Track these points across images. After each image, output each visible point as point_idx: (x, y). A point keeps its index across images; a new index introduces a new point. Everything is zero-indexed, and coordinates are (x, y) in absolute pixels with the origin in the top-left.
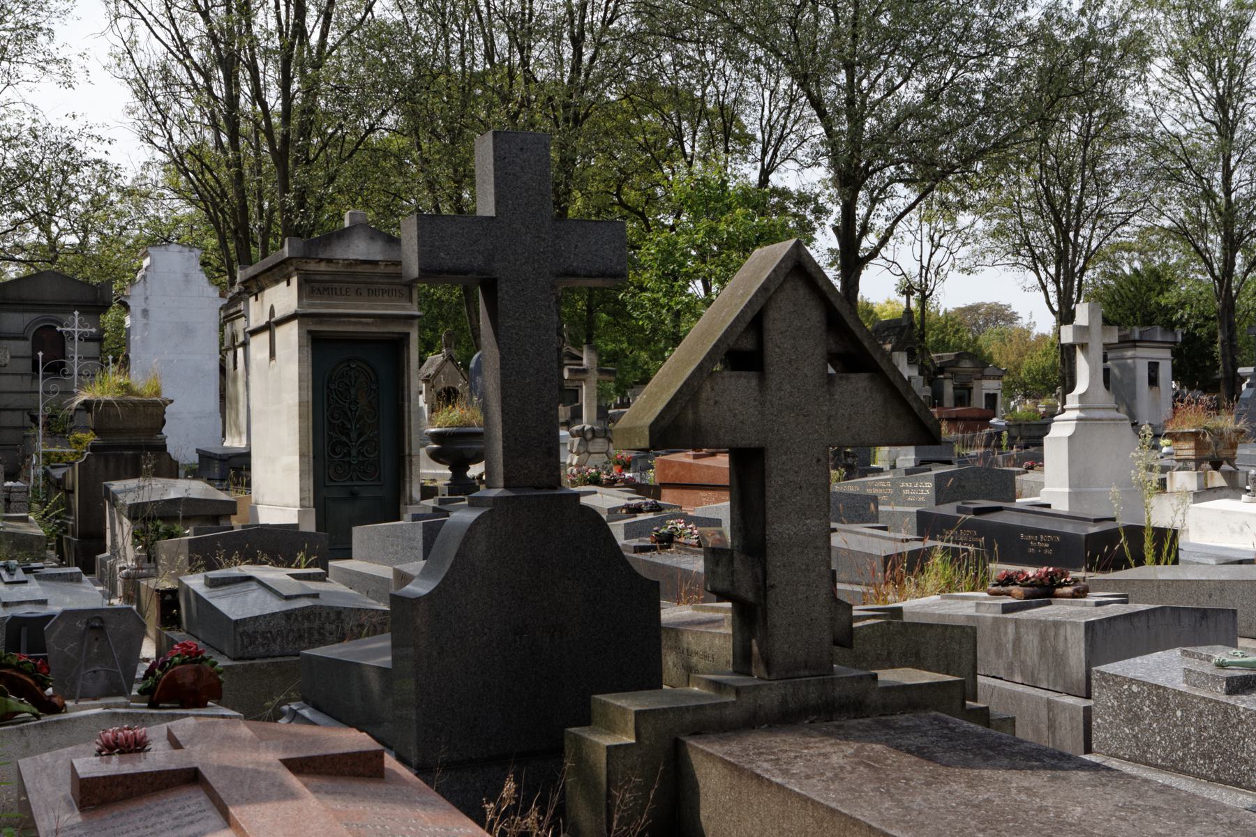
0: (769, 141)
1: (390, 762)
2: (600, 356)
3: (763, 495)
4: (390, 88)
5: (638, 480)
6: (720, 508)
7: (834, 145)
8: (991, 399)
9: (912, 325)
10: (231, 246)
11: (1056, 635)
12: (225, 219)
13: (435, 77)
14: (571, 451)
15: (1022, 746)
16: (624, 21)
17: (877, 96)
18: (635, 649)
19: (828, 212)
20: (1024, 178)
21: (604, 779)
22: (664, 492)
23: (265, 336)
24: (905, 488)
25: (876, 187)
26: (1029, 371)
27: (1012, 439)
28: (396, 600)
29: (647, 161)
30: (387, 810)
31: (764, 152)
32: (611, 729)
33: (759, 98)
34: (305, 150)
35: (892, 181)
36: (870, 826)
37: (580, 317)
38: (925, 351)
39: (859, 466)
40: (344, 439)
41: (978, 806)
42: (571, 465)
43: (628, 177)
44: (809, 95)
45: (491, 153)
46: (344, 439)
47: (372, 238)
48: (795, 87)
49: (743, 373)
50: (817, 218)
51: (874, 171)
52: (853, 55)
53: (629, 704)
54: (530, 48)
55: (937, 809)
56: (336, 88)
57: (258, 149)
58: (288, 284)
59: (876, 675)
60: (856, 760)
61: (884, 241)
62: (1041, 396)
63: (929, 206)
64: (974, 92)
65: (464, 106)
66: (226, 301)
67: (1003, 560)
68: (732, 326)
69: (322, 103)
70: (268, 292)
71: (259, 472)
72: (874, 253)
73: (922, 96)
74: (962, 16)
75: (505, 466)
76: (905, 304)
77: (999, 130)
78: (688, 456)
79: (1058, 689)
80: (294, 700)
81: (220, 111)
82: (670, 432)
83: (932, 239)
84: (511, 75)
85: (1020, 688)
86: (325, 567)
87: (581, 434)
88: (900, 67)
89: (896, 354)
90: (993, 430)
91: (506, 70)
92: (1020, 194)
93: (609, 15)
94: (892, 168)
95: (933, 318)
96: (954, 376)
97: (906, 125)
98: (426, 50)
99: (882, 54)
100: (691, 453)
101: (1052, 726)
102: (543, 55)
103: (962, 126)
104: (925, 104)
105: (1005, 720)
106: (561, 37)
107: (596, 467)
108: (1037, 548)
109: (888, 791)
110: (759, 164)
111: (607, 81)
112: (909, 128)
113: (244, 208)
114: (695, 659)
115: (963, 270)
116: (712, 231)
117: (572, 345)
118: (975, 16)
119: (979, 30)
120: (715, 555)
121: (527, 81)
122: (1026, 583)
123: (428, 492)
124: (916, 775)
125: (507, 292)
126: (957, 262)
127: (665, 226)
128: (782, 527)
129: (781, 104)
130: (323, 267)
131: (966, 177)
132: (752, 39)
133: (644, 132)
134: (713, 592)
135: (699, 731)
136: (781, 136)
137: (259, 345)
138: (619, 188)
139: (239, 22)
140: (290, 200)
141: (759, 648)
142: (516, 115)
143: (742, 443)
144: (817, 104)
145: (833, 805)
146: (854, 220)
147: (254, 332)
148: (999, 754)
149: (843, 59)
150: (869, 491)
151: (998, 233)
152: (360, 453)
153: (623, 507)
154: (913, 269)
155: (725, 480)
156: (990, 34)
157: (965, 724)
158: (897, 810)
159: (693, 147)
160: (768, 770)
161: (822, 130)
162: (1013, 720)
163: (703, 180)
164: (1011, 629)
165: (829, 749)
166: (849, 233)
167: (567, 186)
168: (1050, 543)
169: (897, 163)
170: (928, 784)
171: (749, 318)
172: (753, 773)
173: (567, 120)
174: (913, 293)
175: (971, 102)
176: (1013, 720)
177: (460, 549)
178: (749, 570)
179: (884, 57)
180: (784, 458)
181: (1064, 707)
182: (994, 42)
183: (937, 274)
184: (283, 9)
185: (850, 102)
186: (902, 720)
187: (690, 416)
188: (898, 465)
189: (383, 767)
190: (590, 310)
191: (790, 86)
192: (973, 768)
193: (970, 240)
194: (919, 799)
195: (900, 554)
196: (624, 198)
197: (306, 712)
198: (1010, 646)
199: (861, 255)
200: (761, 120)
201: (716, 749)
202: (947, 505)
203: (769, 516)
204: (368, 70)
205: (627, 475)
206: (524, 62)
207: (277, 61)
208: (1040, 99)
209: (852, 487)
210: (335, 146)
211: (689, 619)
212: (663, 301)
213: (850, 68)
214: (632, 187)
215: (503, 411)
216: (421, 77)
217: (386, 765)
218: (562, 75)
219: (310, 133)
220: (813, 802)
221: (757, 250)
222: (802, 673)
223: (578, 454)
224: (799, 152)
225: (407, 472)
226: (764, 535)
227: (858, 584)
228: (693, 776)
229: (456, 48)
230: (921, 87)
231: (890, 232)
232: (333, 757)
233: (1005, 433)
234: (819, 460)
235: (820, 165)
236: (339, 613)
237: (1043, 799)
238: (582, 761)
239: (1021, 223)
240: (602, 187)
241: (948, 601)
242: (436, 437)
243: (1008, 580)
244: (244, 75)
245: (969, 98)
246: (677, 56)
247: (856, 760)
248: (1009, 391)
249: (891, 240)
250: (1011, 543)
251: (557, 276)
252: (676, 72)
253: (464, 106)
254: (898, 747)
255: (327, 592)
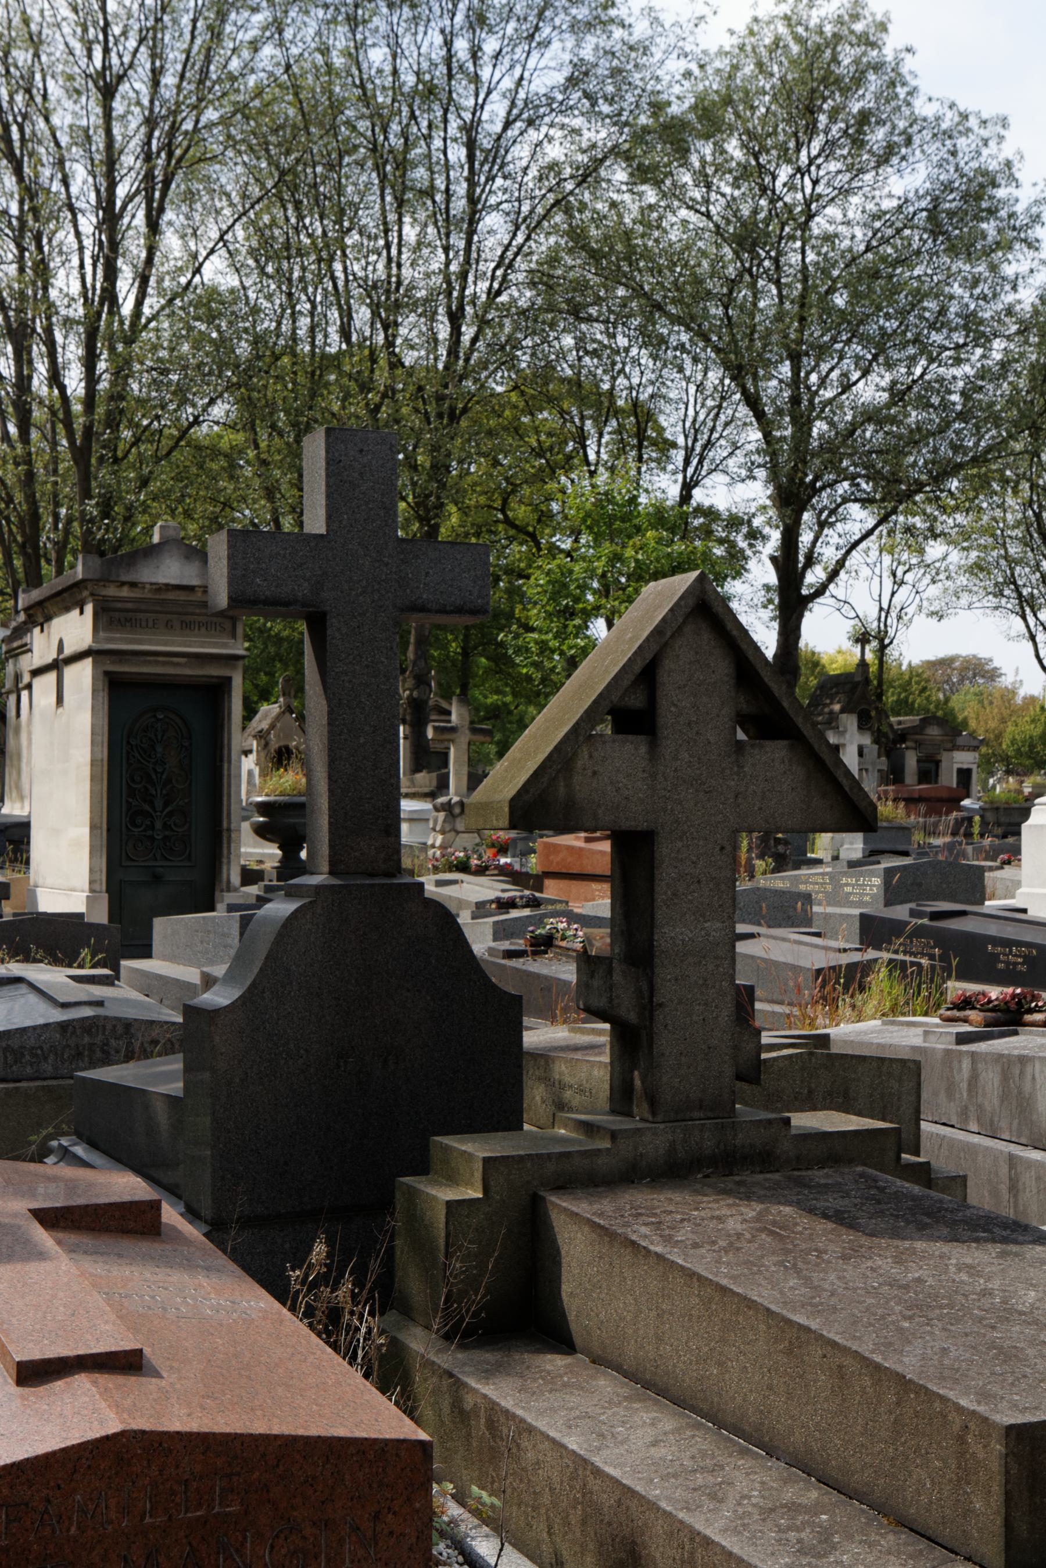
0: (693, 449)
1: (171, 1214)
2: (477, 710)
3: (651, 891)
4: (221, 372)
5: (517, 867)
6: (599, 903)
7: (774, 455)
8: (965, 775)
9: (867, 681)
10: (18, 563)
11: (1022, 1073)
12: (10, 531)
13: (277, 358)
14: (434, 829)
15: (968, 1213)
16: (516, 294)
17: (828, 394)
18: (490, 1080)
19: (765, 538)
20: (1010, 501)
21: (442, 1242)
22: (548, 883)
23: (51, 677)
24: (847, 885)
25: (825, 508)
26: (1013, 741)
27: (984, 823)
28: (190, 1011)
29: (541, 469)
30: (160, 1277)
31: (687, 462)
32: (452, 1179)
33: (683, 393)
34: (111, 445)
35: (845, 500)
36: (768, 1310)
37: (454, 662)
38: (883, 714)
39: (789, 855)
40: (147, 807)
41: (906, 1287)
42: (433, 846)
43: (515, 488)
44: (745, 392)
45: (323, 453)
46: (147, 807)
47: (187, 558)
48: (727, 381)
49: (630, 737)
50: (751, 546)
51: (823, 488)
52: (800, 342)
53: (476, 1149)
54: (396, 324)
55: (855, 1289)
56: (153, 369)
57: (54, 444)
58: (82, 613)
59: (789, 1119)
60: (758, 1225)
61: (833, 576)
62: (1028, 772)
63: (891, 533)
64: (950, 393)
65: (313, 395)
66: (8, 632)
67: (962, 977)
68: (616, 678)
69: (135, 386)
70: (56, 622)
71: (41, 847)
72: (821, 590)
73: (886, 395)
74: (937, 296)
75: (331, 846)
76: (859, 655)
77: (979, 440)
78: (578, 839)
79: (1023, 1141)
80: (64, 1134)
81: (8, 393)
82: (539, 809)
83: (894, 575)
84: (373, 359)
85: (976, 1139)
86: (116, 968)
87: (448, 807)
88: (858, 358)
89: (844, 716)
90: (964, 814)
91: (366, 352)
92: (1005, 521)
93: (496, 285)
94: (846, 484)
95: (894, 672)
96: (919, 745)
97: (864, 431)
98: (266, 324)
99: (836, 342)
100: (583, 835)
101: (1014, 1188)
102: (414, 333)
103: (933, 434)
104: (888, 406)
105: (954, 1178)
106: (435, 313)
107: (465, 850)
108: (1007, 963)
109: (795, 1265)
110: (680, 477)
111: (491, 368)
112: (868, 434)
113: (35, 517)
114: (568, 1094)
115: (932, 614)
116: (616, 558)
117: (442, 697)
118: (951, 297)
119: (957, 314)
120: (586, 960)
121: (392, 366)
122: (988, 1007)
123: (250, 876)
124: (831, 1247)
125: (339, 629)
126: (925, 603)
127: (562, 551)
128: (674, 931)
129: (710, 403)
130: (125, 592)
131: (938, 498)
132: (675, 320)
133: (537, 433)
134: (588, 1010)
135: (564, 1185)
136: (709, 441)
137: (45, 686)
138: (505, 502)
139: (34, 283)
140: (91, 507)
141: (643, 1082)
142: (377, 408)
143: (626, 825)
144: (753, 402)
145: (724, 1282)
146: (797, 548)
147: (36, 673)
148: (937, 1222)
149: (787, 347)
150: (802, 887)
151: (977, 569)
152: (165, 826)
153: (492, 902)
154: (870, 612)
155: (604, 866)
156: (971, 322)
157: (899, 1182)
158: (804, 1290)
159: (598, 453)
160: (646, 1236)
161: (759, 435)
162: (964, 1179)
163: (606, 494)
164: (966, 1064)
165: (725, 1211)
166: (789, 566)
167: (438, 498)
168: (1025, 957)
169: (852, 478)
170: (845, 1258)
171: (638, 668)
172: (626, 1239)
173: (440, 416)
174: (868, 642)
175: (945, 405)
176: (964, 1179)
177: (271, 950)
178: (628, 982)
179: (838, 346)
180: (679, 844)
181: (1030, 1164)
182: (976, 330)
183: (899, 618)
184: (89, 269)
185: (795, 400)
186: (820, 1176)
187: (562, 790)
188: (842, 856)
189: (160, 1223)
190: (466, 653)
191: (722, 381)
192: (904, 1239)
193: (942, 576)
194: (832, 1277)
195: (833, 968)
196: (510, 514)
197: (79, 1150)
198: (964, 1086)
199: (805, 592)
200: (684, 421)
201: (583, 1207)
202: (899, 908)
203: (659, 915)
204: (193, 347)
205: (503, 861)
206: (390, 344)
207: (79, 335)
208: (1032, 402)
209: (780, 882)
210: (151, 442)
211: (563, 1043)
212: (554, 644)
213: (795, 358)
214: (520, 502)
215: (330, 778)
216: (259, 358)
217: (165, 1218)
218: (436, 359)
219: (118, 425)
220: (700, 1278)
221: (652, 584)
222: (696, 1114)
223: (443, 832)
224: (731, 462)
225: (225, 852)
226: (652, 940)
227: (781, 1003)
228: (554, 1241)
229: (304, 322)
230: (883, 384)
231: (841, 564)
232: (97, 1206)
233: (977, 818)
234: (722, 848)
235: (755, 478)
236: (128, 1025)
237: (988, 1279)
238: (415, 1221)
239: (1006, 557)
240: (482, 500)
241: (891, 1028)
242: (264, 808)
243: (966, 1003)
244: (38, 349)
245: (943, 399)
246: (581, 341)
247: (758, 1225)
248: (987, 766)
249: (842, 573)
250: (975, 957)
251: (402, 610)
252: (580, 359)
253: (313, 395)
254: (811, 1211)
255: (115, 999)
